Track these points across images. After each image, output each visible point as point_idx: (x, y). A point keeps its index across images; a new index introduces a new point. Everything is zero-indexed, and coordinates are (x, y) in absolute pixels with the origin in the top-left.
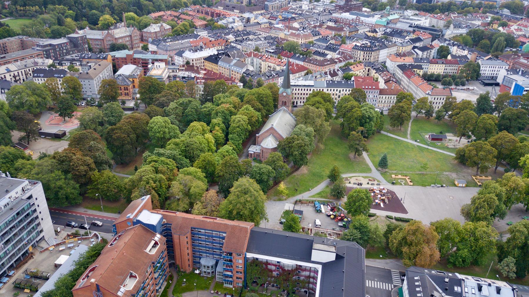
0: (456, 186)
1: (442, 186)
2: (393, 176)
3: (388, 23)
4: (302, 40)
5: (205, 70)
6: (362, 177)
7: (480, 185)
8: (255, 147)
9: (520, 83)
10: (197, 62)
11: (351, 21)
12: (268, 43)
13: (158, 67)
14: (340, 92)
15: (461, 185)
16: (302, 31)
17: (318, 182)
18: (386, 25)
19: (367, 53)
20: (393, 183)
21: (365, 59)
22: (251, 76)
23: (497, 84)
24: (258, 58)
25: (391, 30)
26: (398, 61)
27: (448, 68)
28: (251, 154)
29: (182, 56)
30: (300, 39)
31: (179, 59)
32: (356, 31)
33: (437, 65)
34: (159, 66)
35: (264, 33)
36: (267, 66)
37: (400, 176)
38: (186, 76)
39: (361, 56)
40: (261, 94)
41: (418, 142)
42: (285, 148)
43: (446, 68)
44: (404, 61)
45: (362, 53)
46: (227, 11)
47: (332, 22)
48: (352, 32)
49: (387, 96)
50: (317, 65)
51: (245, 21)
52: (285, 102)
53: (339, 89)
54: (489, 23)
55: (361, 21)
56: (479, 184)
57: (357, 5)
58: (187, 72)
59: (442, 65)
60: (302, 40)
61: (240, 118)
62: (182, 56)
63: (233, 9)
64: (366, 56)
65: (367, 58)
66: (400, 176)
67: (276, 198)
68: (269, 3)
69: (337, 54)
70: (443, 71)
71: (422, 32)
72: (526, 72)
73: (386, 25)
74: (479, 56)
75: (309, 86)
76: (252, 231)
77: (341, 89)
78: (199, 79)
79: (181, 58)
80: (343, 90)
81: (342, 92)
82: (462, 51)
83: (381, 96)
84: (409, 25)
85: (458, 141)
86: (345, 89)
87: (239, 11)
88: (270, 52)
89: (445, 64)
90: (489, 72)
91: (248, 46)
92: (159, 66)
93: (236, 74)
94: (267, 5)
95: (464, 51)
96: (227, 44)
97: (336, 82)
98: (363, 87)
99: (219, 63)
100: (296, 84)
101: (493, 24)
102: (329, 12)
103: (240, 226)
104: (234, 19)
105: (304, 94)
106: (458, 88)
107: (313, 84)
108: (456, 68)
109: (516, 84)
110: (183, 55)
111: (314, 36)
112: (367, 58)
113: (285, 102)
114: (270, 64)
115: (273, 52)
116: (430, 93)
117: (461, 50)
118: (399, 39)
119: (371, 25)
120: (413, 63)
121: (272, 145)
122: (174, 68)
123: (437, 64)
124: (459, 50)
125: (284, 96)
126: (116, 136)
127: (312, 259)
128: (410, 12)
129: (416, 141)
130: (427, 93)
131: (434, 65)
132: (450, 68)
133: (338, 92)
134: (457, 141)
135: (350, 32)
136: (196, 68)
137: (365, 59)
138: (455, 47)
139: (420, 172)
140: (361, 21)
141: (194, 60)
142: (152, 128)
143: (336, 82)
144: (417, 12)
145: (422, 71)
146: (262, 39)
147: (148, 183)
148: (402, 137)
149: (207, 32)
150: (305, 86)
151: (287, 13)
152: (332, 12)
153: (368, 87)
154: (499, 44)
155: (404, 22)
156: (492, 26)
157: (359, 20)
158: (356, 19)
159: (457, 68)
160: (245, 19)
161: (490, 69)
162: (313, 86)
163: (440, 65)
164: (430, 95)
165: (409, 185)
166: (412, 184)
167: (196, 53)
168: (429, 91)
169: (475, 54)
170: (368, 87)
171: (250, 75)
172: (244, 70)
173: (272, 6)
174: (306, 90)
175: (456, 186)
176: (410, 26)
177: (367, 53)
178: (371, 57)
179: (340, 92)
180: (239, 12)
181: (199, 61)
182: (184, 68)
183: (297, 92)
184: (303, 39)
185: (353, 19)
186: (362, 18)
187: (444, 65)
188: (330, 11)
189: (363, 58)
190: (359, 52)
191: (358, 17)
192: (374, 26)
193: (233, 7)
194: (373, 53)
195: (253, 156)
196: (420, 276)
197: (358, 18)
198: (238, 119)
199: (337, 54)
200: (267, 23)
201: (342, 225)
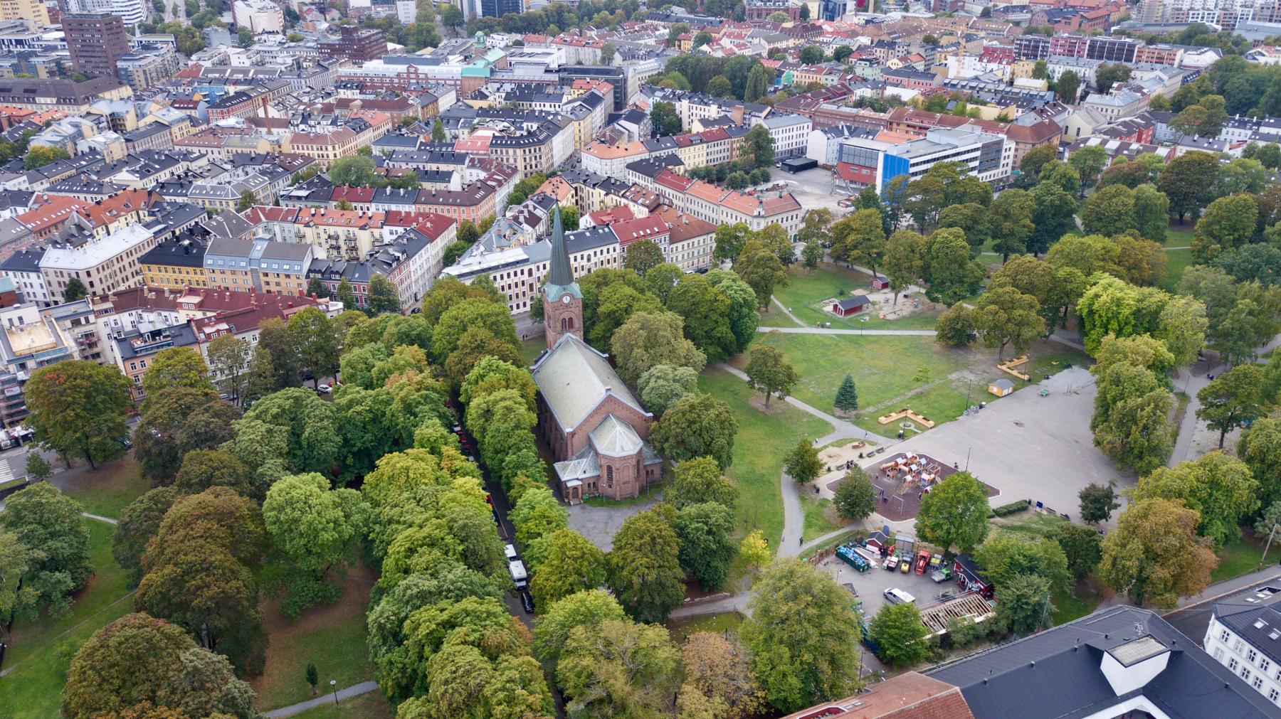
0: (999, 397)
1: (981, 407)
2: (882, 419)
3: (492, 71)
4: (334, 149)
5: (192, 292)
6: (832, 445)
7: (1029, 380)
8: (575, 467)
9: (894, 152)
10: (102, 275)
11: (396, 80)
12: (263, 173)
13: (16, 322)
14: (589, 260)
15: (1006, 392)
16: (302, 127)
17: (774, 495)
18: (488, 75)
19: (530, 151)
20: (900, 436)
21: (528, 167)
22: (341, 275)
23: (813, 165)
24: (284, 220)
25: (513, 86)
26: (616, 155)
27: (713, 149)
28: (575, 488)
29: (37, 269)
30: (330, 148)
31: (26, 280)
32: (433, 103)
33: (692, 148)
34: (20, 319)
35: (216, 150)
36: (324, 236)
37: (894, 416)
38: (159, 326)
39: (518, 160)
40: (488, 315)
41: (828, 327)
42: (683, 441)
43: (709, 150)
44: (628, 152)
45: (519, 152)
46: (19, 106)
47: (351, 88)
48: (427, 106)
49: (685, 243)
50: (458, 205)
51: (105, 124)
52: (571, 319)
53: (586, 253)
54: (668, 40)
55: (421, 76)
56: (1026, 377)
57: (373, 38)
58: (126, 314)
59: (701, 146)
60: (334, 149)
61: (503, 399)
62: (37, 269)
63: (32, 95)
64: (531, 159)
65: (533, 163)
66: (894, 416)
67: (746, 578)
68: (130, 63)
69: (468, 167)
70: (704, 159)
71: (588, 80)
72: (856, 128)
73: (488, 75)
74: (748, 111)
75: (518, 262)
76: (962, 691)
77: (591, 252)
78: (208, 325)
79: (33, 275)
80: (595, 253)
81: (593, 260)
82: (703, 107)
83: (674, 246)
84: (543, 68)
85: (892, 302)
86: (598, 250)
87: (54, 100)
88: (299, 198)
89: (707, 142)
90: (784, 142)
91: (214, 194)
92: (20, 319)
93: (282, 280)
94: (125, 70)
95: (707, 108)
96: (153, 201)
97: (588, 234)
98: (635, 235)
99: (208, 261)
100: (485, 266)
101: (680, 41)
102: (320, 65)
103: (937, 699)
104: (76, 126)
105: (516, 285)
106: (759, 188)
107: (525, 257)
108: (727, 146)
109: (887, 157)
110: (43, 263)
111: (358, 133)
112: (533, 163)
113: (571, 319)
114: (331, 230)
115: (306, 197)
116: (762, 213)
117: (699, 107)
118: (547, 104)
119: (452, 82)
120: (646, 156)
121: (634, 443)
122: (75, 314)
123: (692, 145)
124: (695, 106)
125: (567, 305)
126: (211, 598)
127: (1119, 692)
128: (500, 37)
129: (823, 326)
130: (756, 213)
131: (687, 149)
132: (716, 148)
133: (584, 262)
134: (887, 301)
135: (423, 108)
136: (152, 295)
137: (528, 167)
138: (685, 103)
139: (913, 392)
140: (421, 76)
141: (93, 272)
142: (296, 521)
143: (588, 234)
144: (519, 37)
145: (682, 167)
146: (228, 167)
147: (510, 701)
148: (788, 327)
149: (25, 178)
150: (507, 265)
151: (206, 85)
152: (325, 64)
153: (652, 230)
154: (756, 80)
155: (530, 64)
156: (680, 46)
157: (416, 72)
158: (409, 73)
159: (729, 146)
160: (103, 119)
161: (785, 135)
162: (526, 261)
163: (697, 147)
164: (763, 217)
165: (928, 429)
166: (931, 423)
167: (89, 246)
168: (758, 210)
169: (740, 109)
170: (652, 230)
171: (337, 273)
172: (307, 265)
173: (144, 71)
174: (512, 275)
175: (999, 397)
176: (546, 71)
177: (530, 151)
178: (540, 158)
179: (589, 260)
180: (58, 103)
181: (107, 272)
182: (109, 305)
183: (506, 281)
184: (337, 146)
185: (398, 75)
186: (423, 69)
187: (705, 145)
188: (322, 63)
189: (523, 164)
190: (511, 151)
191: (411, 66)
192: (458, 82)
193: (26, 91)
194: (542, 147)
195: (580, 491)
196: (1261, 617)
197: (412, 70)
198: (503, 404)
199: (468, 167)
200: (182, 120)
201: (943, 577)
